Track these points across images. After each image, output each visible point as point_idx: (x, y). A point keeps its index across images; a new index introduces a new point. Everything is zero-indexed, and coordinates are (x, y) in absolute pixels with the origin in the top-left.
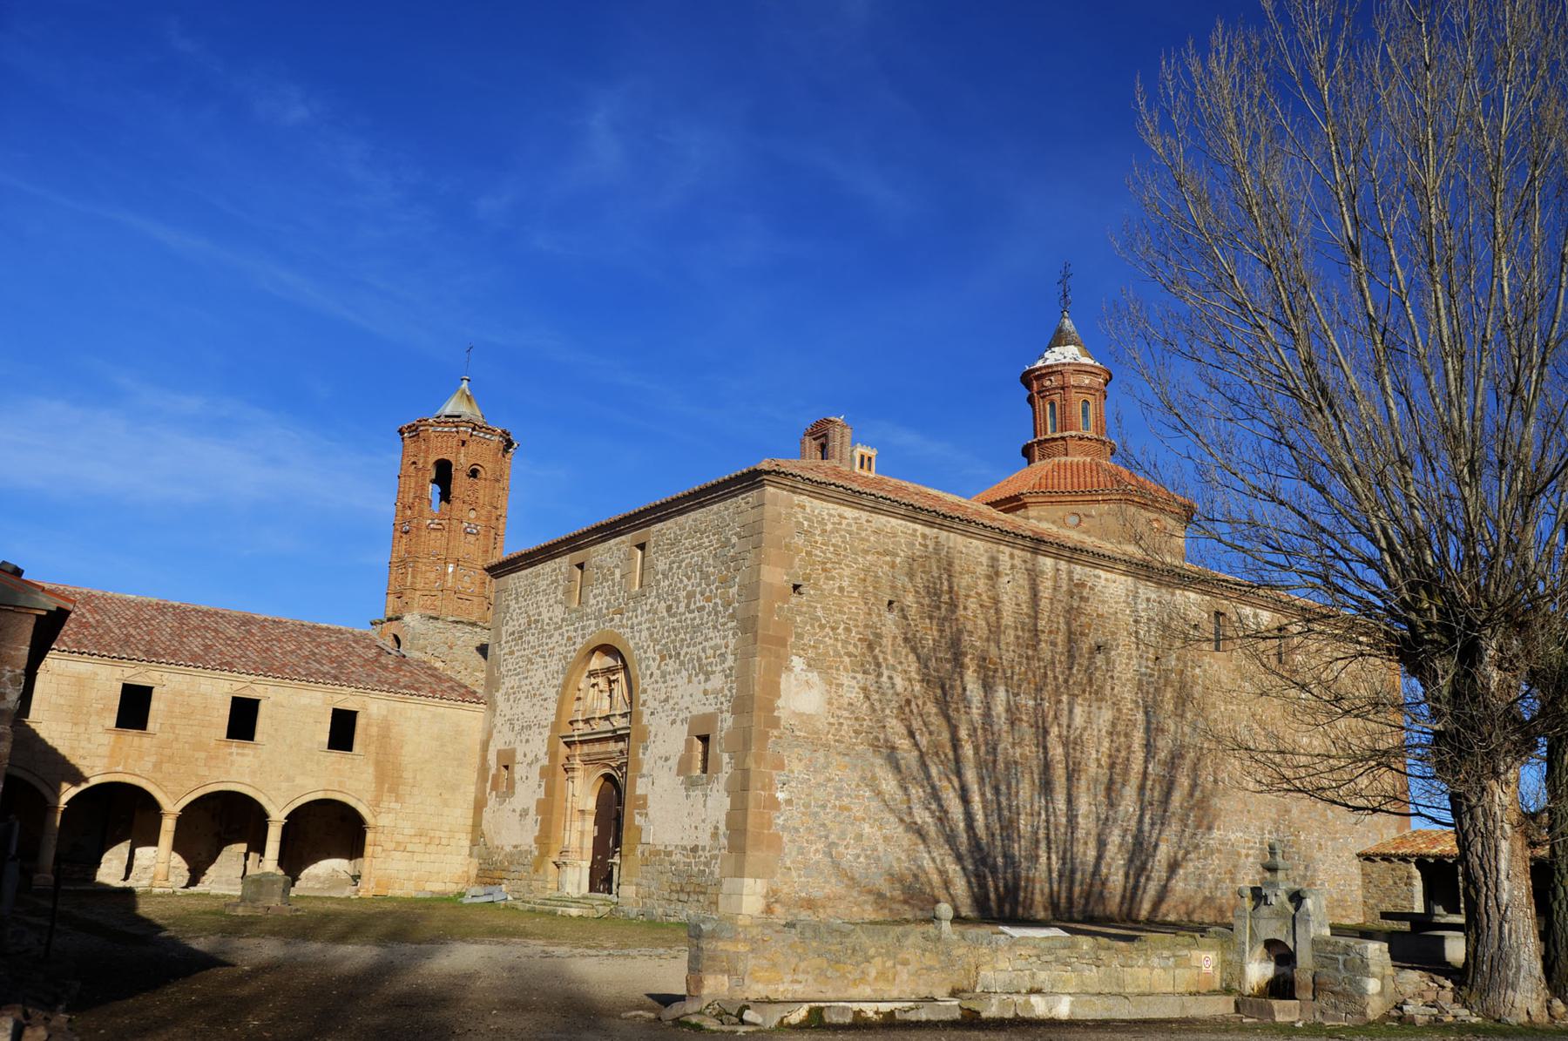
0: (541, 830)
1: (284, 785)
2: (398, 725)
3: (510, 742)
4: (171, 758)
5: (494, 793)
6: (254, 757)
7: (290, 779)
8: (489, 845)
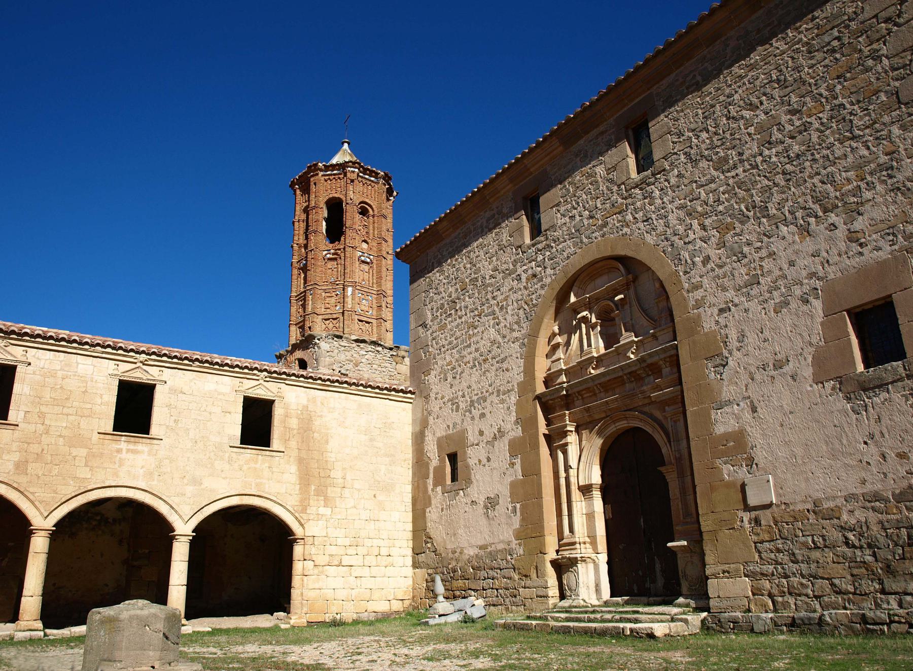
0: (523, 519)
1: (189, 490)
2: (321, 416)
3: (455, 425)
4: (39, 457)
5: (439, 489)
6: (149, 454)
7: (196, 482)
8: (440, 549)
